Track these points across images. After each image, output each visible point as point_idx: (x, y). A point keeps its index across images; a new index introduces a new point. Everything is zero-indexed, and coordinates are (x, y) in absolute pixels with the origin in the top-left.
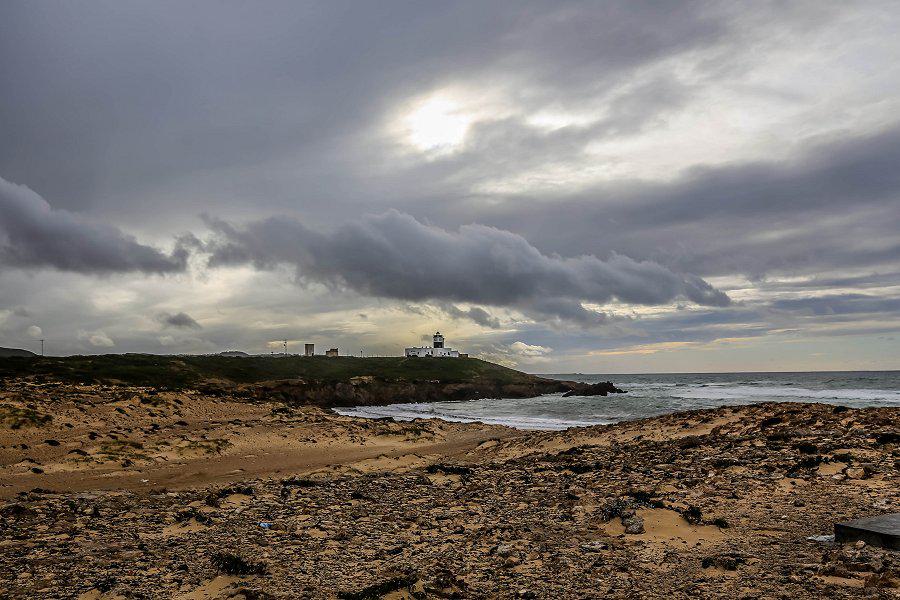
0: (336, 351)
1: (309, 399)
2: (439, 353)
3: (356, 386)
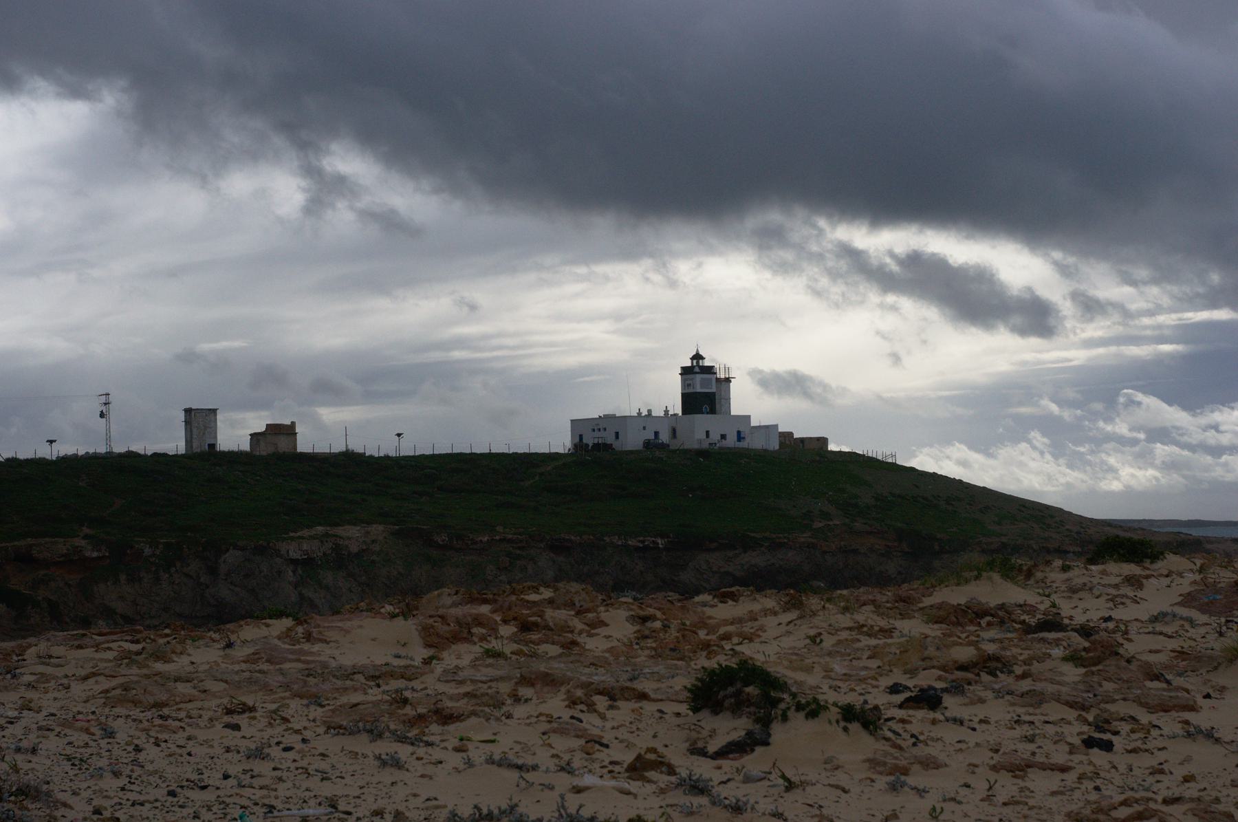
0: (288, 431)
1: (108, 613)
2: (702, 429)
3: (308, 563)
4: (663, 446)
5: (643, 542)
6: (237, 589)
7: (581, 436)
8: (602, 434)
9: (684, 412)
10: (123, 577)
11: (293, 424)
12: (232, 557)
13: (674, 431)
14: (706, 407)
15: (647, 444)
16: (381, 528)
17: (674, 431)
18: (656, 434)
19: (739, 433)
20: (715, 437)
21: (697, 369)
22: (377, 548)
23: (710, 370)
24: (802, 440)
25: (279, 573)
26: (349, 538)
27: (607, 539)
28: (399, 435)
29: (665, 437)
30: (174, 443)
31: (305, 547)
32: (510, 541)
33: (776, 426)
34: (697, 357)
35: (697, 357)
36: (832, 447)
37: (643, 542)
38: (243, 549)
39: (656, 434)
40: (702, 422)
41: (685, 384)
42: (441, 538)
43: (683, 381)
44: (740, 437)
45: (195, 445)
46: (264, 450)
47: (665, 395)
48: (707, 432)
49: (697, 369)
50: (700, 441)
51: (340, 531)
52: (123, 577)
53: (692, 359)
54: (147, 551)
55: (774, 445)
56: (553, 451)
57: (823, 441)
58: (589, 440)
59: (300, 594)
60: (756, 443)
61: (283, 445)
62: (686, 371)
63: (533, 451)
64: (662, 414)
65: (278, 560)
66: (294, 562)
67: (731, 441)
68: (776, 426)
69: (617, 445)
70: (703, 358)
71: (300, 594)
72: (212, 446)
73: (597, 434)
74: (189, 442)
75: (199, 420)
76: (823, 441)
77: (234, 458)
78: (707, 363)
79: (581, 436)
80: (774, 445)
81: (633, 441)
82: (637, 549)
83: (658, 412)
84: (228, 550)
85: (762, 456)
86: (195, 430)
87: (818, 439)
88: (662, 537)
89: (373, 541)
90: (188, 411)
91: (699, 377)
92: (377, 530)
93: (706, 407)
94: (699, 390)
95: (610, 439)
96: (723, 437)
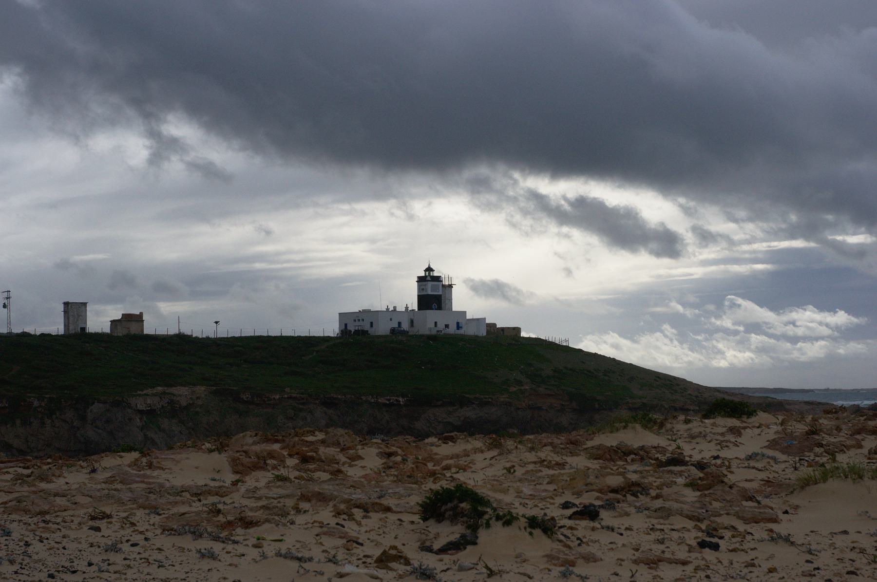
2: (432, 321)
3: (150, 413)
4: (404, 333)
5: (389, 400)
6: (100, 431)
7: (346, 325)
8: (361, 323)
9: (419, 309)
10: (18, 422)
11: (141, 314)
12: (96, 408)
13: (412, 322)
14: (435, 305)
15: (393, 331)
16: (203, 388)
17: (412, 322)
18: (400, 323)
19: (458, 323)
20: (441, 326)
21: (429, 278)
22: (200, 402)
23: (438, 279)
24: (503, 329)
25: (130, 419)
26: (180, 396)
27: (364, 398)
28: (216, 322)
29: (405, 326)
30: (56, 326)
31: (149, 402)
32: (295, 398)
34: (429, 269)
36: (524, 334)
37: (389, 400)
38: (104, 402)
39: (400, 323)
40: (432, 316)
42: (245, 396)
44: (458, 327)
45: (71, 327)
46: (120, 332)
47: (405, 296)
48: (372, 323)
49: (429, 278)
50: (430, 329)
51: (173, 390)
52: (18, 422)
53: (426, 271)
54: (36, 403)
55: (483, 332)
56: (326, 335)
57: (517, 330)
58: (352, 328)
59: (146, 436)
60: (469, 331)
61: (134, 329)
62: (421, 280)
64: (404, 310)
65: (129, 411)
66: (141, 412)
67: (452, 330)
69: (372, 332)
70: (433, 270)
71: (146, 436)
72: (83, 329)
73: (357, 323)
74: (66, 326)
75: (74, 310)
76: (517, 330)
77: (98, 337)
78: (436, 274)
79: (346, 325)
80: (483, 332)
81: (383, 328)
82: (385, 405)
83: (401, 308)
84: (93, 403)
85: (474, 340)
86: (71, 319)
87: (514, 328)
88: (403, 397)
89: (198, 398)
90: (66, 304)
91: (430, 284)
92: (201, 390)
93: (435, 305)
94: (430, 293)
95: (367, 327)
96: (447, 326)
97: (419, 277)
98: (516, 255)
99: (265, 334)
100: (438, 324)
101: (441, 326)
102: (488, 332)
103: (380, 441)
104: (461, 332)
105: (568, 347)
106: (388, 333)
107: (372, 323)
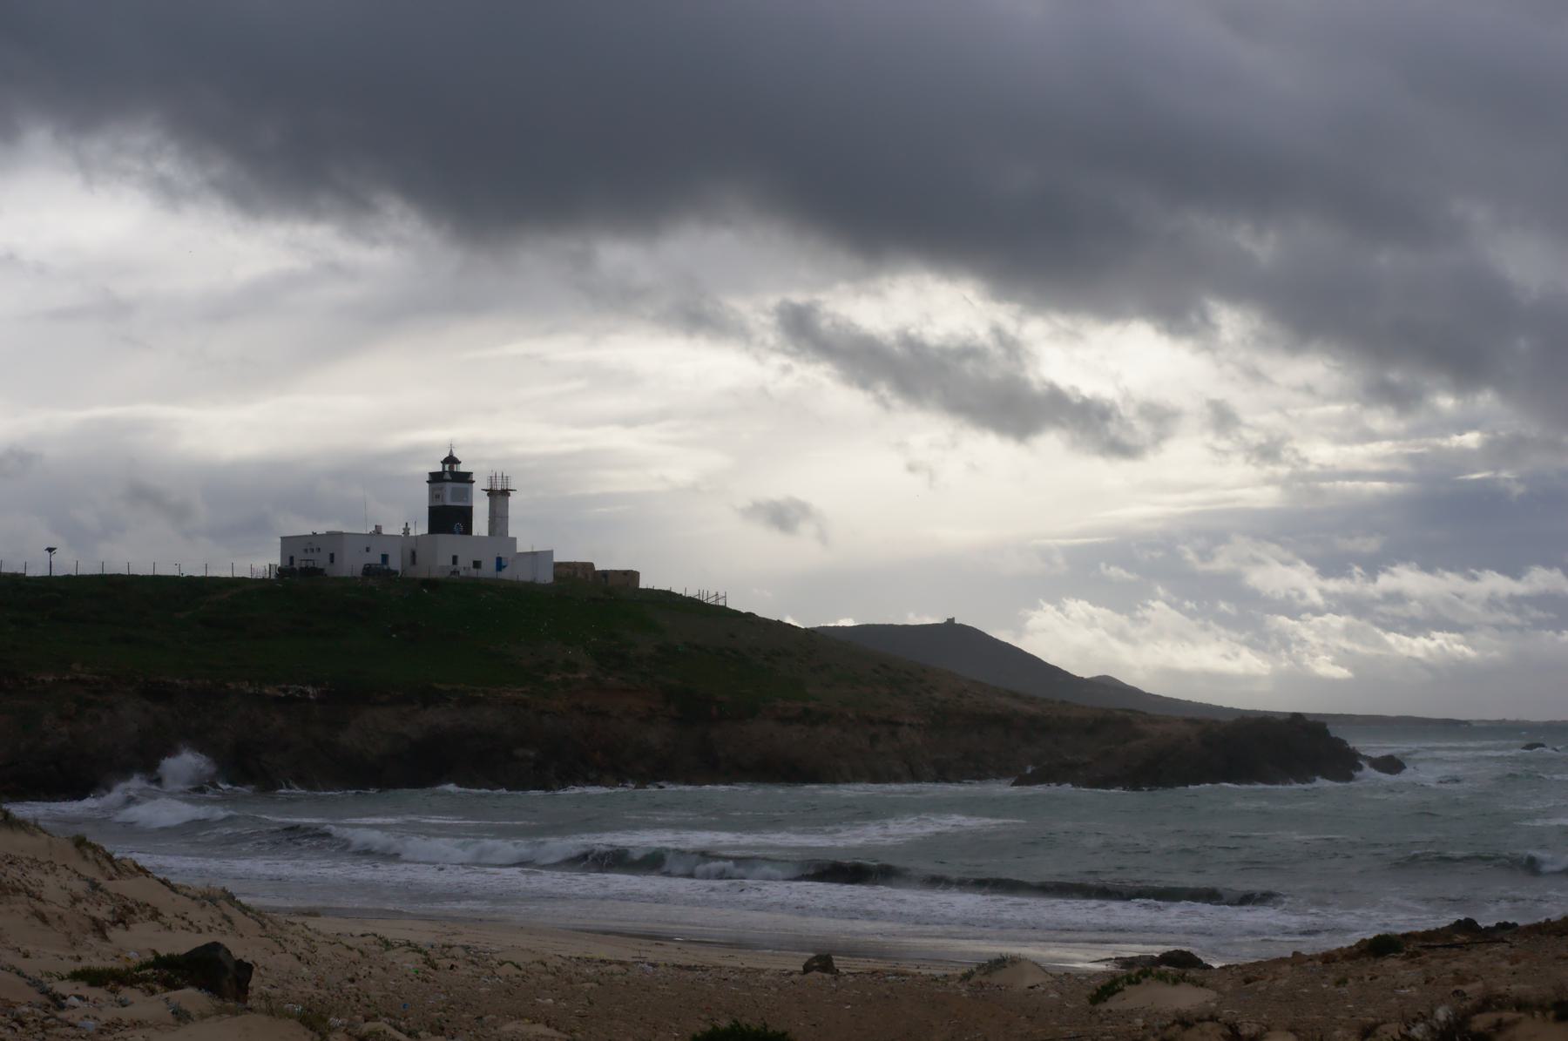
2: (446, 554)
5: (285, 691)
7: (292, 558)
15: (368, 570)
18: (385, 558)
19: (499, 560)
21: (448, 476)
24: (605, 574)
27: (232, 685)
28: (50, 550)
29: (395, 564)
33: (551, 553)
34: (451, 460)
35: (451, 460)
36: (644, 584)
37: (285, 691)
39: (385, 558)
40: (449, 544)
41: (434, 495)
43: (432, 491)
44: (500, 565)
47: (406, 515)
48: (332, 556)
49: (448, 476)
53: (445, 462)
55: (547, 577)
56: (237, 574)
60: (522, 573)
62: (435, 478)
63: (107, 572)
64: (400, 532)
67: (488, 570)
68: (551, 553)
69: (332, 571)
76: (632, 576)
78: (462, 468)
79: (292, 558)
80: (547, 577)
81: (351, 564)
82: (277, 699)
83: (393, 529)
84: (145, 760)
87: (626, 573)
88: (314, 685)
91: (449, 486)
94: (449, 503)
95: (321, 561)
97: (432, 474)
98: (721, 429)
99: (124, 572)
100: (459, 560)
101: (465, 562)
102: (555, 576)
103: (1467, 989)
104: (505, 574)
105: (724, 608)
106: (358, 572)
107: (332, 556)
